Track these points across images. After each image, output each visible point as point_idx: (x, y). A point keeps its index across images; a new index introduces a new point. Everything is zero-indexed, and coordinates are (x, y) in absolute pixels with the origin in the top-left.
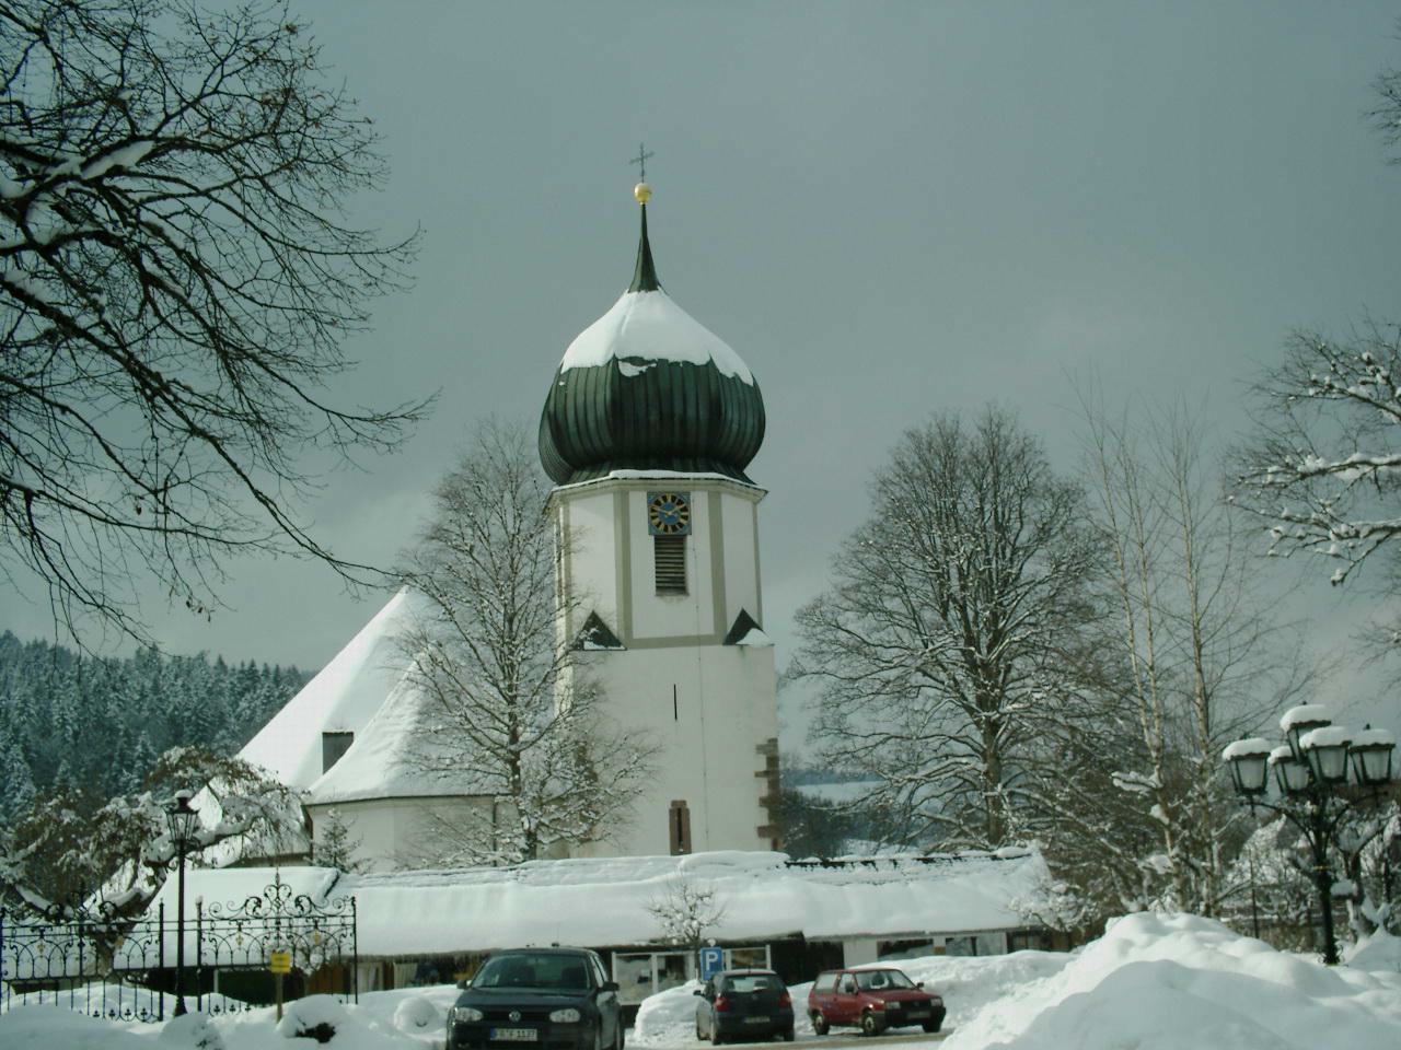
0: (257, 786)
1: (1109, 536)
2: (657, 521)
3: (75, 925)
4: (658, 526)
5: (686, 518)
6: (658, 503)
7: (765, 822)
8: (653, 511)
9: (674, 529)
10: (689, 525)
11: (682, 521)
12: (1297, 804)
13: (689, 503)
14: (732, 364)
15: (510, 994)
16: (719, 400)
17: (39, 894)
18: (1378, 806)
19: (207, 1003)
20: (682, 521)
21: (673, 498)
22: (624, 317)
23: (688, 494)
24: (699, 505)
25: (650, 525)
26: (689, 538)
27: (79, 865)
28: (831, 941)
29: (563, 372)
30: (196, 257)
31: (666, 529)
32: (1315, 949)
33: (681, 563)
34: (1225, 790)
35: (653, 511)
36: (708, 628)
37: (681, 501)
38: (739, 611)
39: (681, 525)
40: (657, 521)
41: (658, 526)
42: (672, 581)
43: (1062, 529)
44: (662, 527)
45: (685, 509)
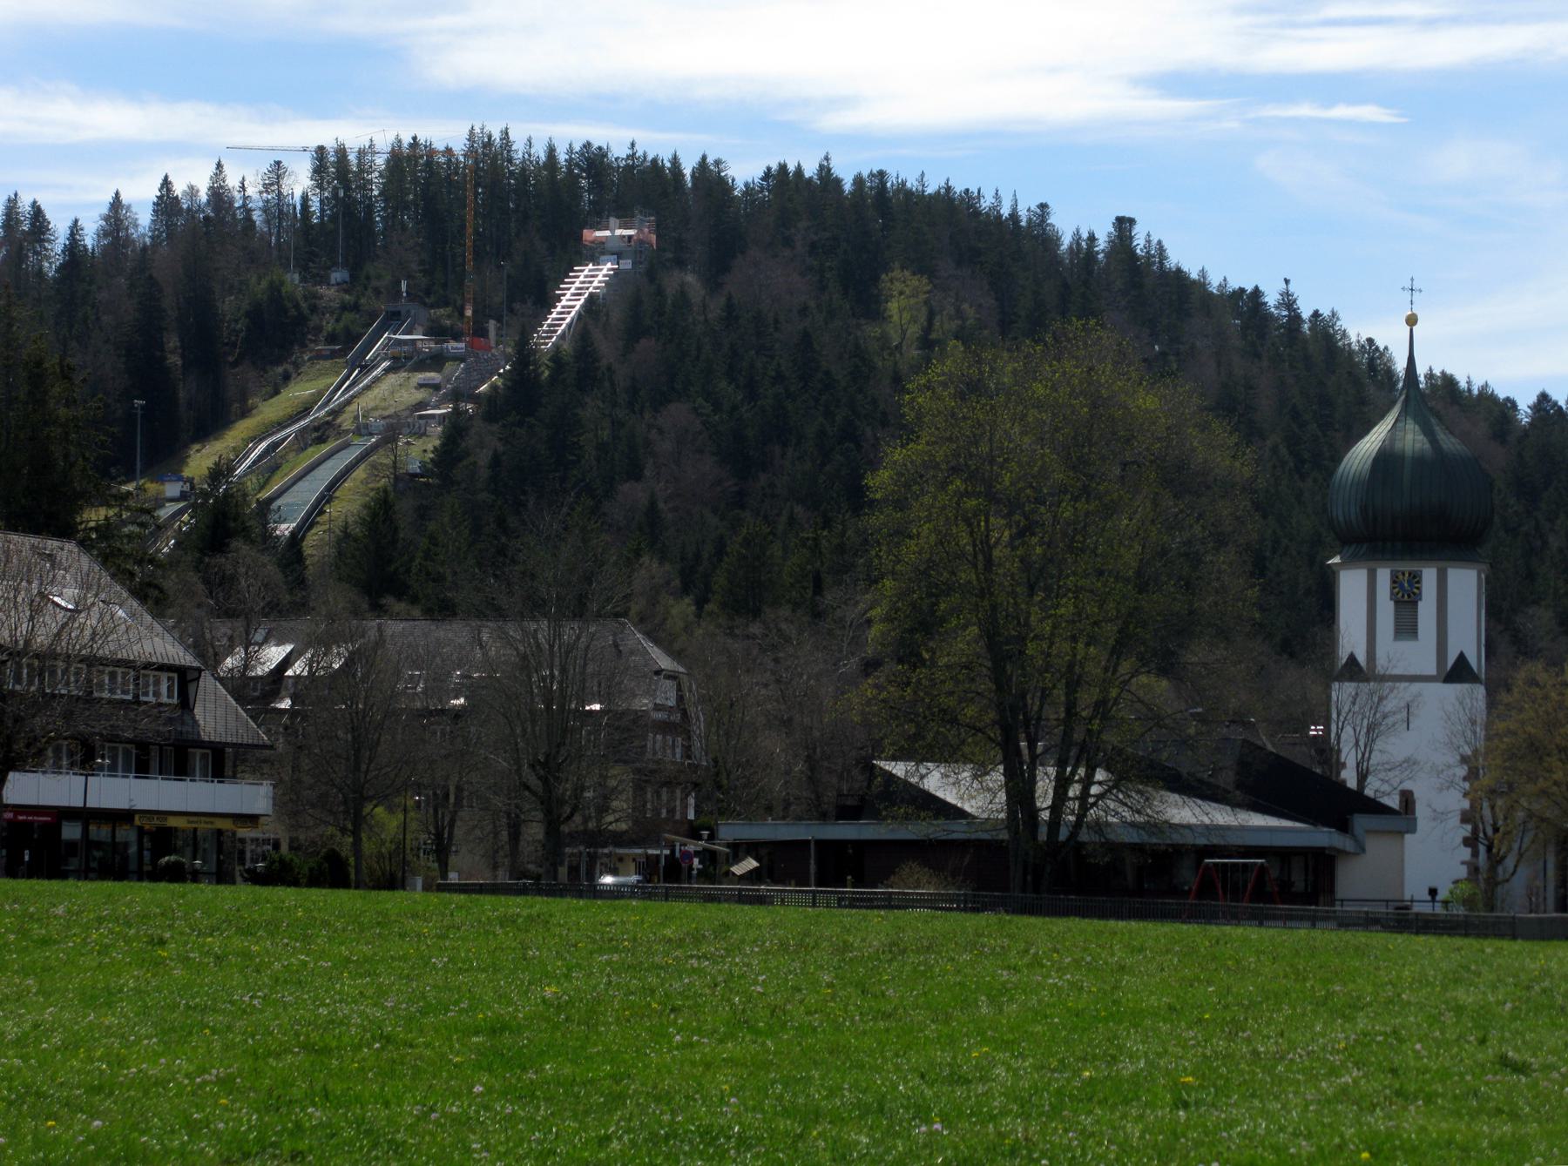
1: (773, 1011)
2: (1397, 590)
3: (1084, 709)
4: (1398, 594)
5: (1418, 588)
6: (1415, 577)
8: (1418, 588)
9: (1409, 596)
10: (1420, 594)
11: (1415, 590)
13: (1421, 577)
17: (195, 877)
18: (558, 348)
20: (1415, 590)
24: (1429, 576)
25: (1392, 594)
26: (1419, 602)
28: (1336, 627)
30: (1343, 760)
31: (1403, 596)
34: (332, 339)
36: (1431, 669)
37: (1415, 578)
39: (1414, 594)
40: (1397, 590)
41: (1398, 594)
42: (1406, 627)
43: (1139, 812)
44: (1400, 595)
45: (1418, 582)
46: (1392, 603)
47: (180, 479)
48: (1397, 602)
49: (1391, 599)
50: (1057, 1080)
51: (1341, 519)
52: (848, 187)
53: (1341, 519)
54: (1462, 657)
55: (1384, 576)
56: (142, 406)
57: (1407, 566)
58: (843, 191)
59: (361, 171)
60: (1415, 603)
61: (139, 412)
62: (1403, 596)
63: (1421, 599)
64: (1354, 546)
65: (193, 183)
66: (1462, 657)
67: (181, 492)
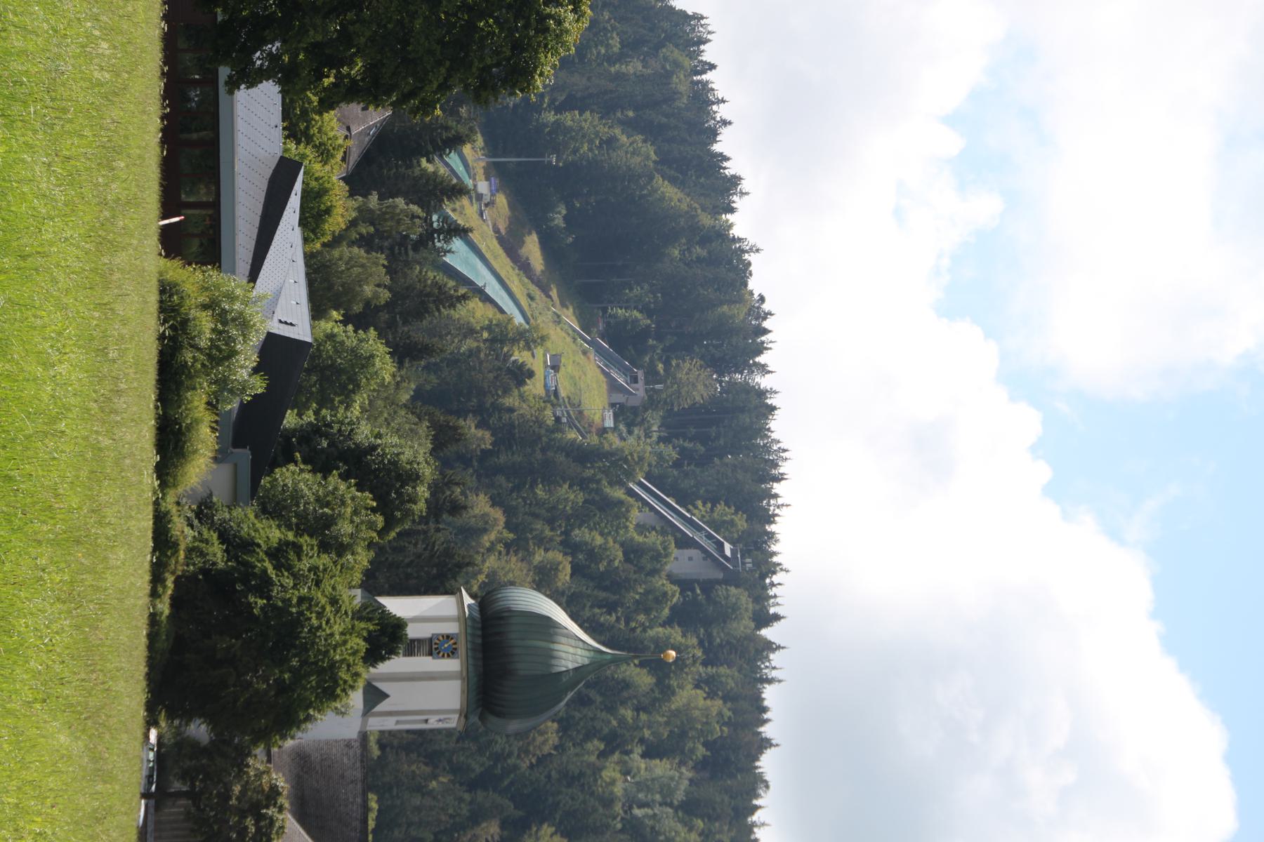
0: (598, 735)
2: (441, 638)
4: (438, 639)
6: (453, 653)
7: (725, 164)
9: (436, 649)
10: (439, 658)
12: (328, 343)
13: (453, 658)
14: (372, 670)
15: (672, 517)
16: (783, 479)
19: (566, 650)
21: (455, 649)
22: (600, 367)
23: (458, 658)
24: (452, 665)
25: (438, 635)
27: (672, 675)
29: (503, 232)
31: (436, 644)
32: (444, 732)
33: (362, 725)
35: (443, 656)
37: (452, 653)
38: (388, 692)
39: (439, 653)
40: (441, 638)
41: (438, 639)
44: (438, 642)
45: (448, 656)
46: (430, 636)
47: (493, 195)
48: (431, 640)
49: (433, 635)
50: (42, 494)
51: (500, 596)
52: (768, 528)
53: (500, 596)
54: (385, 696)
55: (452, 628)
56: (551, 162)
57: (462, 650)
58: (758, 727)
59: (750, 366)
60: (430, 654)
61: (546, 160)
62: (436, 644)
63: (434, 658)
64: (477, 608)
65: (733, 125)
66: (385, 696)
67: (482, 194)
